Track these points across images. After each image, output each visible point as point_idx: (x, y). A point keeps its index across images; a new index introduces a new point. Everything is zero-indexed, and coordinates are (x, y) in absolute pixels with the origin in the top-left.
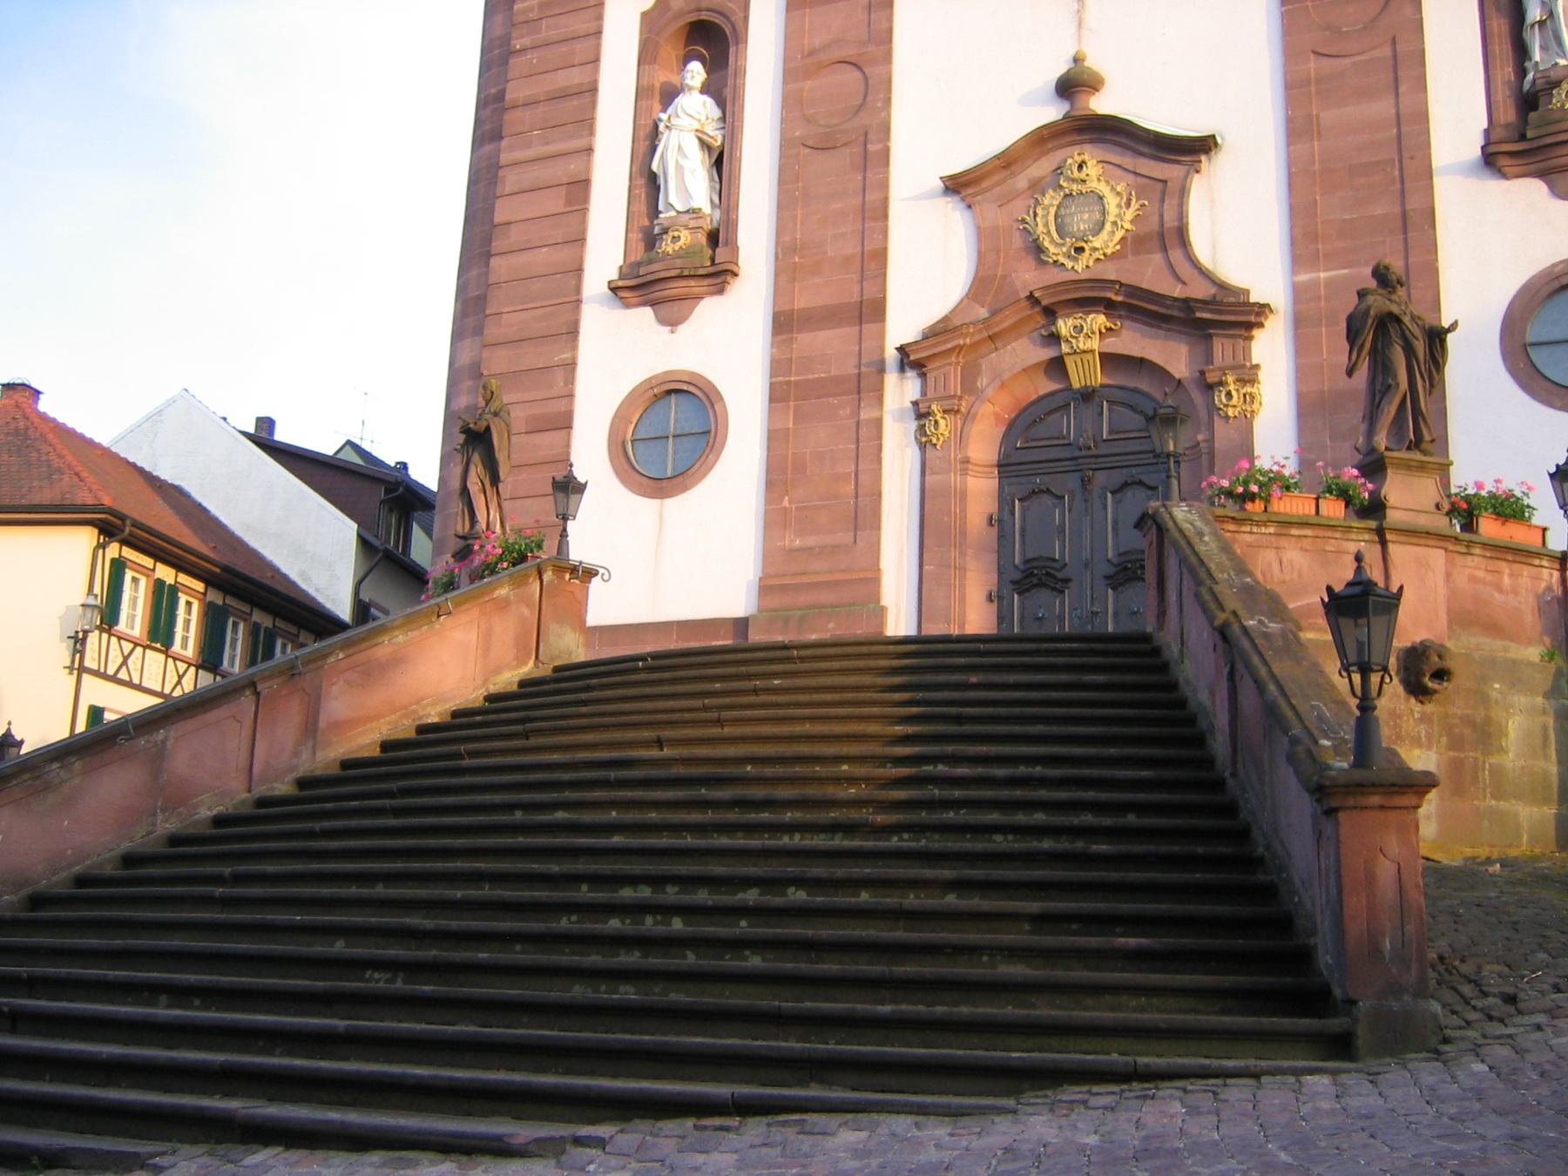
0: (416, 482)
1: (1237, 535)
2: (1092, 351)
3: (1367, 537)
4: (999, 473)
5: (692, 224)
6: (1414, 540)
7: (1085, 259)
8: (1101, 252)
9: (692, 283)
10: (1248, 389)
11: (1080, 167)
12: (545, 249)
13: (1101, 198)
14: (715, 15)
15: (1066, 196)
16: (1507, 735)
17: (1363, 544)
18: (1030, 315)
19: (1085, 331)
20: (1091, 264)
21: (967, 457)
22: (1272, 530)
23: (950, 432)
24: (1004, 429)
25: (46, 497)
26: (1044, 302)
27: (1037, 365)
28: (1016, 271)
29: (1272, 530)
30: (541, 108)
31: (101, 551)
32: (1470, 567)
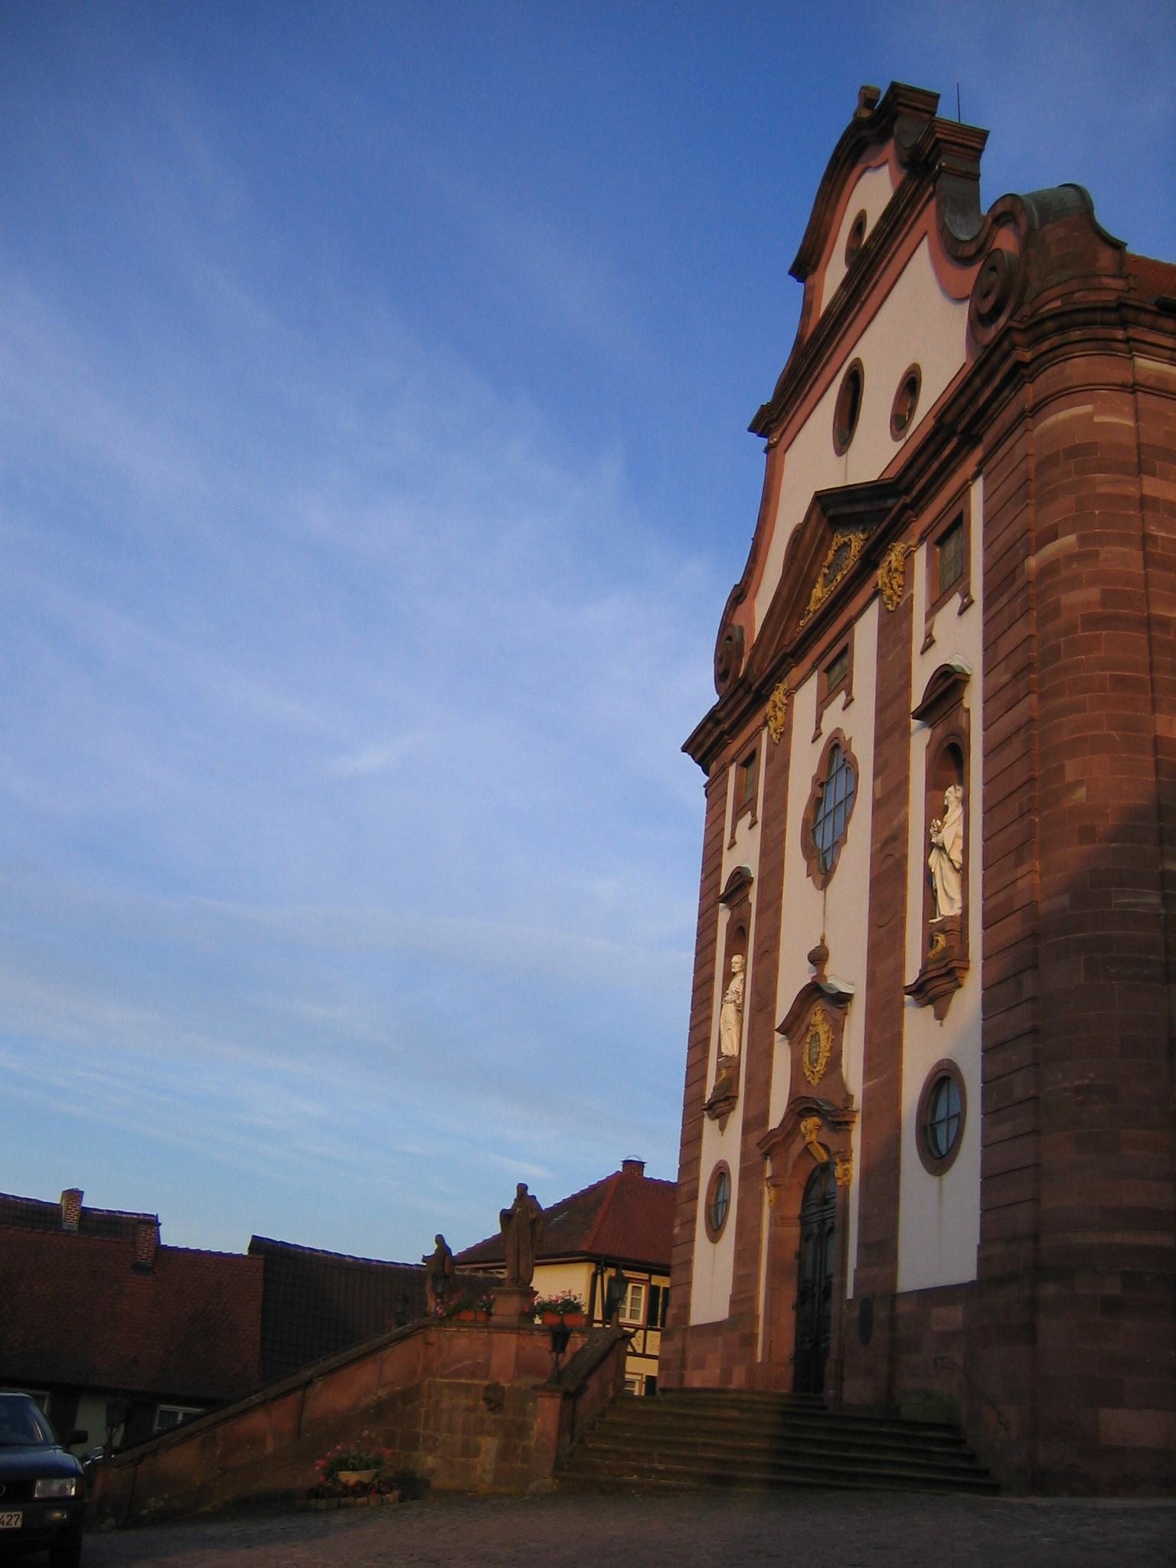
31: (599, 1277)
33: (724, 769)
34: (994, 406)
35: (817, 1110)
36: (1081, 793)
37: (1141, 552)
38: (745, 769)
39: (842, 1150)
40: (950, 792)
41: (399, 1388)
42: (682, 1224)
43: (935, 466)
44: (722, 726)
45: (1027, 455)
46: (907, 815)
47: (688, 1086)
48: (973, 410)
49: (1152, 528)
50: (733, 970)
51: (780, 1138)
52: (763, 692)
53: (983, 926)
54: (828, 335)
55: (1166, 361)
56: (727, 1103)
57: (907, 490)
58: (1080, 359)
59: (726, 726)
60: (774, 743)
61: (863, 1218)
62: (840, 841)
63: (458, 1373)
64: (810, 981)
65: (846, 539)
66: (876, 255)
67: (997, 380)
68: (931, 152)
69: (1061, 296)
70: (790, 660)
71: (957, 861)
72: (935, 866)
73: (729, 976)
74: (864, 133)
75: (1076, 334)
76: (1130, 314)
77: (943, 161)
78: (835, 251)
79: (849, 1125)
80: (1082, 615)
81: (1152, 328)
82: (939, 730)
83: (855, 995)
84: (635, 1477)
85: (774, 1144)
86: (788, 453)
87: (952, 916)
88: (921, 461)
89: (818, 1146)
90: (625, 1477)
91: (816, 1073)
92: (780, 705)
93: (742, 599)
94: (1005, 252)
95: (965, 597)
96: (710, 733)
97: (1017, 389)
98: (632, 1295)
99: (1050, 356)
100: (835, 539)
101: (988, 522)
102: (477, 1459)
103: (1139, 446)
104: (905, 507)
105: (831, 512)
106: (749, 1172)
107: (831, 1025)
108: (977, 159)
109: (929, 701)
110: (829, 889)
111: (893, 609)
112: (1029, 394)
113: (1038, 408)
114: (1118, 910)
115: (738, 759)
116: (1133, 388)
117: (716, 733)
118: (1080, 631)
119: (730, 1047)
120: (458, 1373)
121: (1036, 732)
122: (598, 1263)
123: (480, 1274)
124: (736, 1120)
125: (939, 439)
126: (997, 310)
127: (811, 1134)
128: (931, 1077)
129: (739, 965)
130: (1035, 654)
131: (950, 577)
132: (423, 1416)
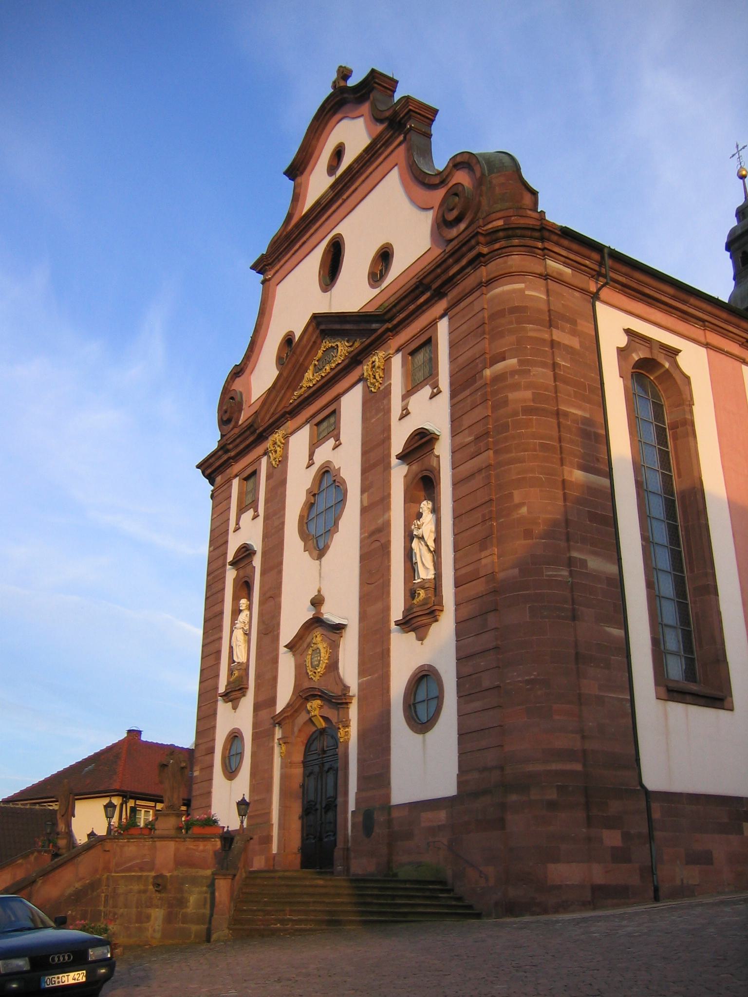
0: (719, 613)
4: (304, 765)
5: (239, 668)
10: (347, 730)
16: (189, 902)
22: (126, 841)
25: (101, 788)
29: (126, 841)
31: (124, 805)
33: (229, 481)
34: (459, 277)
35: (320, 696)
36: (524, 510)
37: (552, 373)
38: (245, 482)
39: (344, 720)
40: (424, 505)
41: (88, 881)
42: (201, 770)
43: (412, 307)
44: (230, 453)
45: (483, 309)
46: (390, 516)
47: (202, 682)
48: (444, 277)
49: (558, 359)
50: (241, 608)
51: (289, 714)
52: (264, 434)
53: (455, 586)
54: (316, 216)
55: (562, 263)
56: (240, 692)
57: (390, 320)
58: (517, 256)
59: (232, 454)
60: (274, 467)
61: (361, 762)
62: (332, 529)
63: (129, 869)
64: (312, 617)
65: (333, 345)
66: (357, 172)
67: (464, 262)
68: (404, 117)
69: (504, 217)
70: (288, 415)
71: (431, 546)
72: (417, 549)
73: (236, 612)
74: (346, 95)
75: (516, 241)
76: (546, 234)
77: (413, 124)
78: (319, 162)
79: (348, 705)
80: (522, 406)
81: (557, 244)
82: (415, 467)
83: (348, 626)
84: (279, 925)
85: (285, 717)
86: (278, 286)
87: (429, 579)
88: (403, 303)
89: (319, 718)
90: (272, 926)
91: (317, 673)
92: (279, 443)
93: (240, 374)
94: (466, 187)
95: (435, 388)
96: (220, 457)
97: (475, 269)
98: (144, 816)
99: (500, 251)
100: (324, 344)
101: (452, 346)
102: (148, 924)
103: (549, 311)
104: (388, 330)
105: (323, 327)
106: (261, 736)
107: (327, 644)
108: (431, 125)
109: (407, 451)
110: (323, 559)
111: (375, 391)
112: (483, 272)
113: (490, 282)
114: (547, 578)
115: (241, 475)
116: (546, 277)
117: (225, 457)
118: (521, 415)
119: (240, 656)
120: (129, 869)
121: (492, 472)
122: (124, 796)
123: (37, 807)
124: (248, 702)
125: (417, 292)
126: (458, 220)
127: (315, 710)
128: (414, 675)
129: (245, 605)
130: (491, 427)
131: (420, 376)
132: (103, 899)
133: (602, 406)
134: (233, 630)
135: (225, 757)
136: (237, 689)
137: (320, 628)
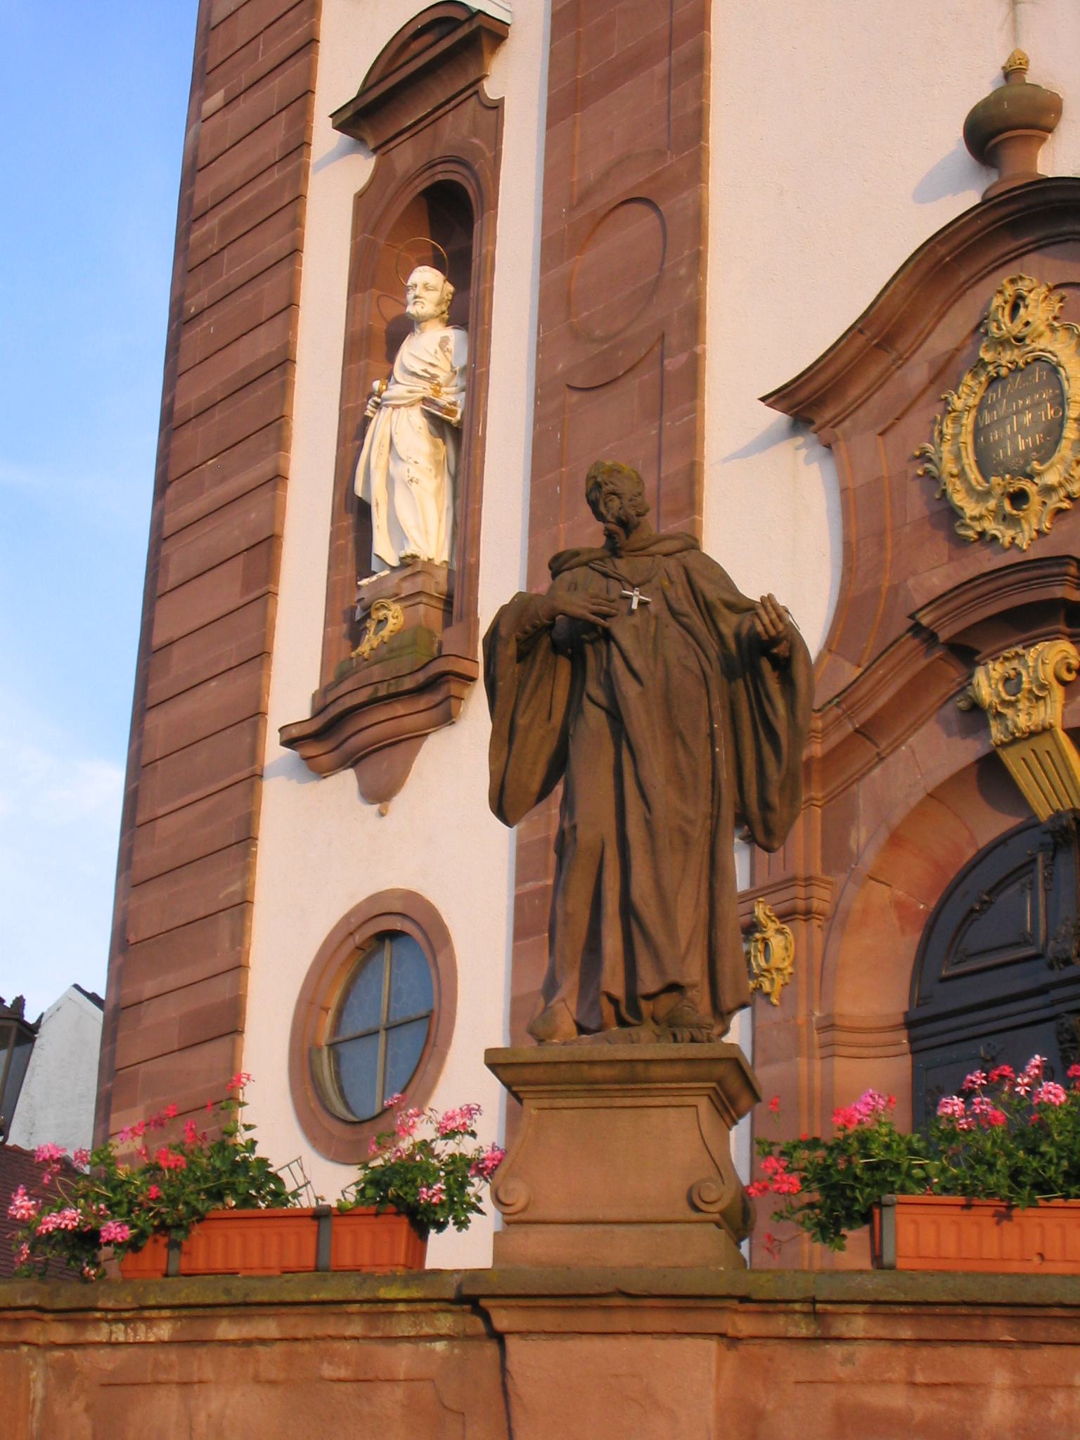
1: (76, 1354)
2: (1046, 730)
3: (445, 1323)
4: (912, 1040)
5: (407, 589)
6: (593, 1320)
7: (1035, 517)
8: (1062, 493)
9: (400, 709)
11: (1015, 309)
12: (213, 683)
13: (1054, 369)
14: (451, 167)
15: (992, 381)
17: (440, 1346)
18: (927, 668)
19: (1025, 686)
20: (1046, 525)
21: (829, 1016)
22: (164, 1331)
23: (793, 964)
24: (917, 937)
26: (944, 635)
27: (956, 779)
28: (914, 573)
29: (164, 1331)
30: (218, 415)
32: (839, 1382)
50: (411, 309)
56: (423, 702)
133: (278, 422)
134: (367, 420)
135: (314, 1050)
136: (408, 684)
137: (1032, 259)
